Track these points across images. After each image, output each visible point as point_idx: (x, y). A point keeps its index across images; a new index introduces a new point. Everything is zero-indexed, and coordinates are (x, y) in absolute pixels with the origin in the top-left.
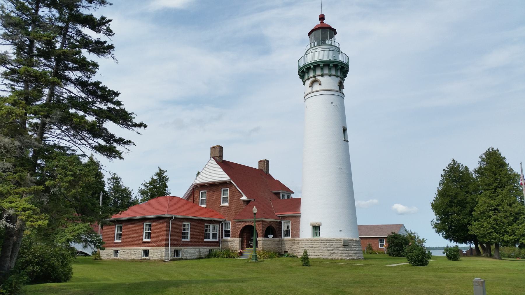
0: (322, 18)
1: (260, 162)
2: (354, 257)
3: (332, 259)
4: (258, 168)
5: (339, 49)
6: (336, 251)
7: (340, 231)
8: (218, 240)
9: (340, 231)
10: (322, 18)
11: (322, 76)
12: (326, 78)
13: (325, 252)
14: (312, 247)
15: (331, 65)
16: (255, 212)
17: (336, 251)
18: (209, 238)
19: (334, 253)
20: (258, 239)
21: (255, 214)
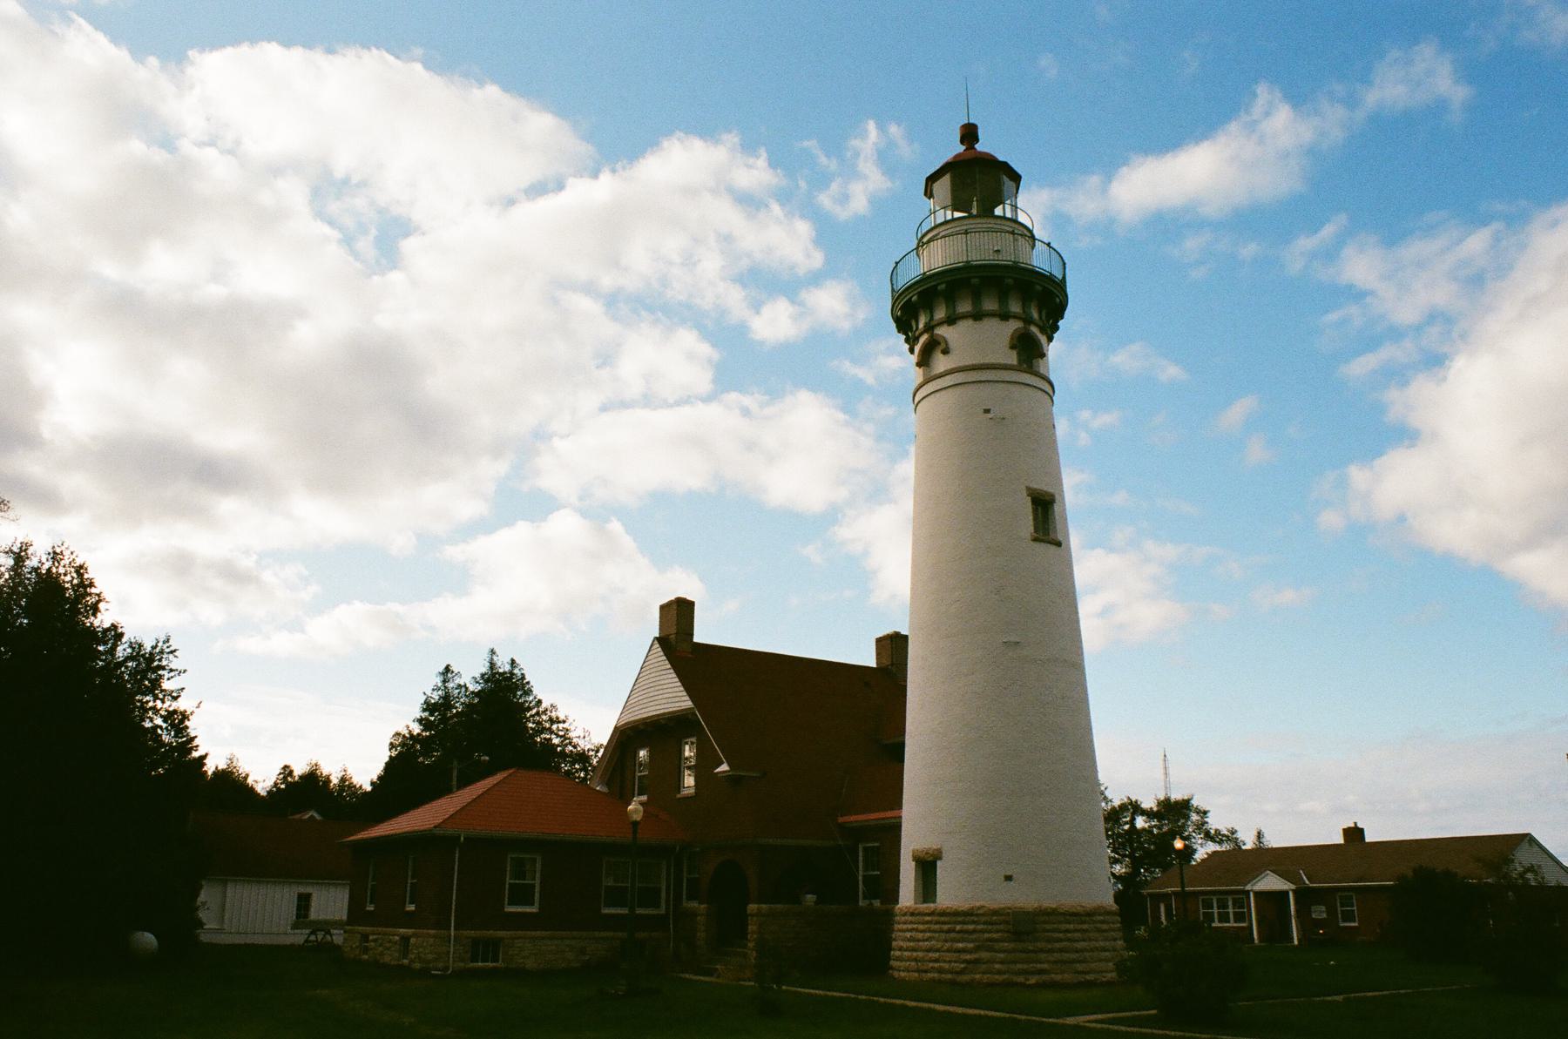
0: (969, 134)
1: (879, 641)
2: (1058, 977)
3: (970, 984)
4: (874, 665)
5: (1031, 231)
6: (984, 955)
7: (1009, 878)
8: (662, 911)
9: (1009, 878)
10: (969, 134)
11: (951, 321)
12: (964, 326)
13: (948, 956)
14: (911, 939)
15: (975, 281)
16: (638, 817)
17: (984, 955)
18: (658, 906)
19: (976, 961)
20: (752, 907)
21: (635, 824)
